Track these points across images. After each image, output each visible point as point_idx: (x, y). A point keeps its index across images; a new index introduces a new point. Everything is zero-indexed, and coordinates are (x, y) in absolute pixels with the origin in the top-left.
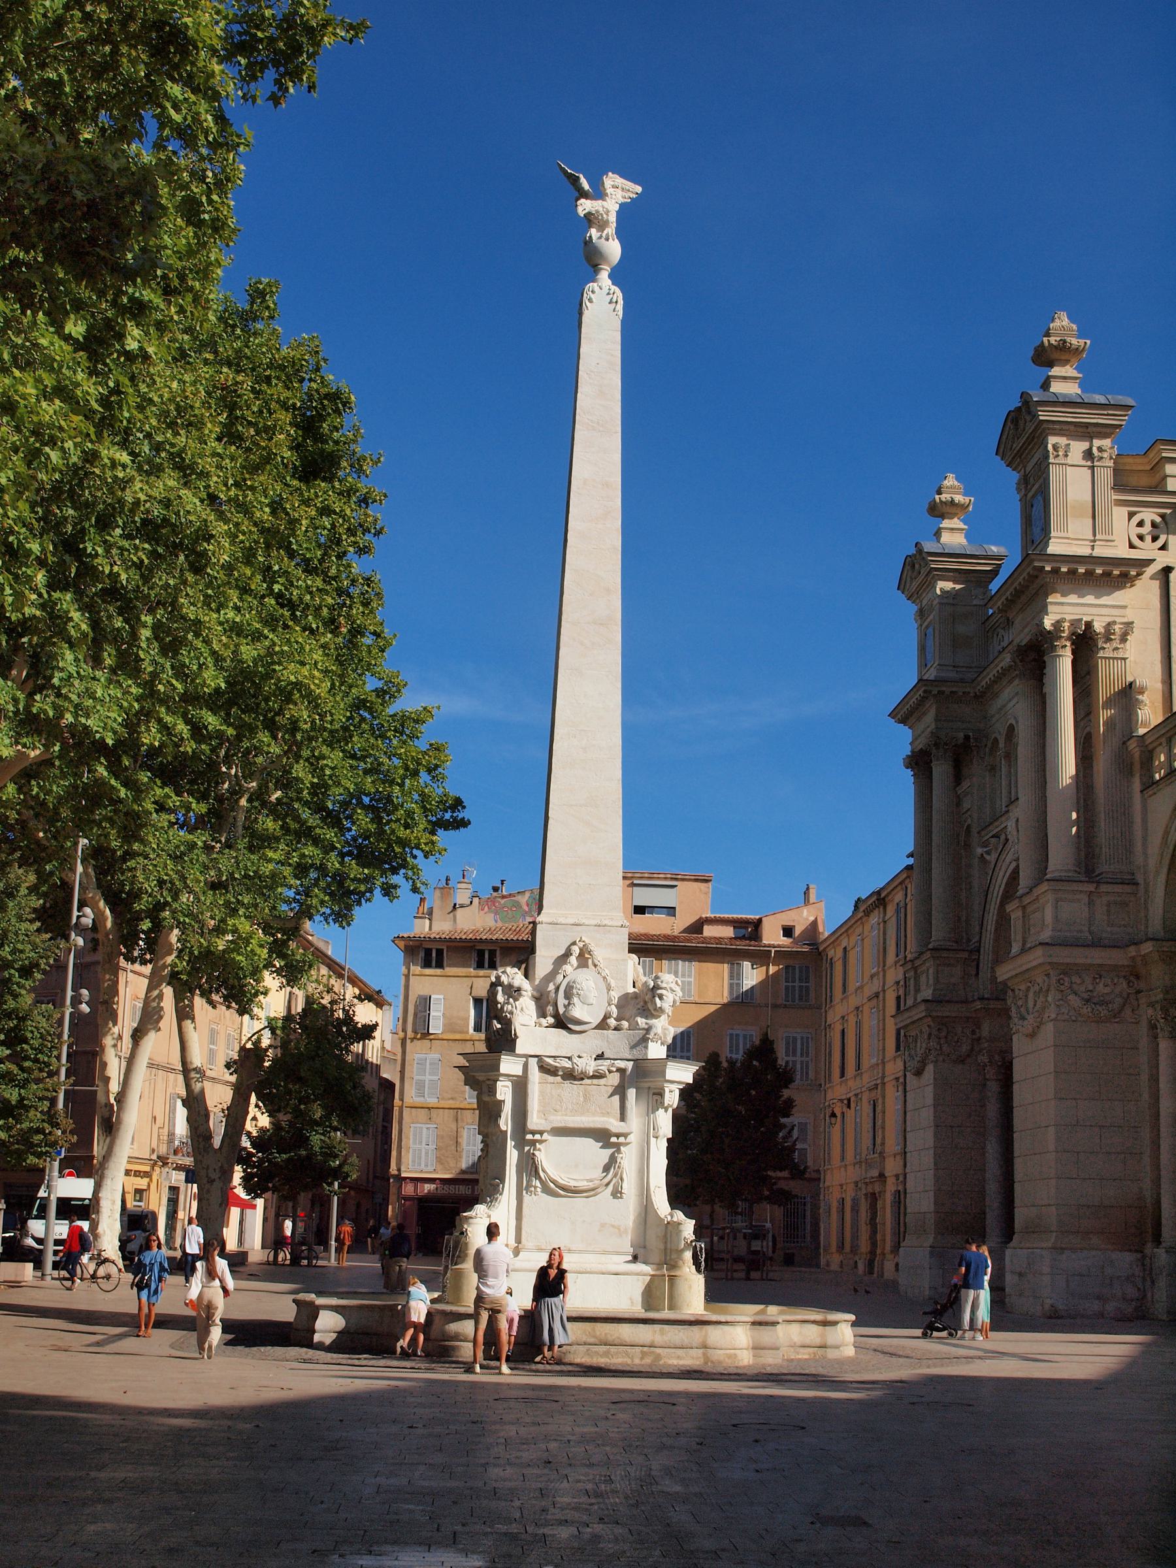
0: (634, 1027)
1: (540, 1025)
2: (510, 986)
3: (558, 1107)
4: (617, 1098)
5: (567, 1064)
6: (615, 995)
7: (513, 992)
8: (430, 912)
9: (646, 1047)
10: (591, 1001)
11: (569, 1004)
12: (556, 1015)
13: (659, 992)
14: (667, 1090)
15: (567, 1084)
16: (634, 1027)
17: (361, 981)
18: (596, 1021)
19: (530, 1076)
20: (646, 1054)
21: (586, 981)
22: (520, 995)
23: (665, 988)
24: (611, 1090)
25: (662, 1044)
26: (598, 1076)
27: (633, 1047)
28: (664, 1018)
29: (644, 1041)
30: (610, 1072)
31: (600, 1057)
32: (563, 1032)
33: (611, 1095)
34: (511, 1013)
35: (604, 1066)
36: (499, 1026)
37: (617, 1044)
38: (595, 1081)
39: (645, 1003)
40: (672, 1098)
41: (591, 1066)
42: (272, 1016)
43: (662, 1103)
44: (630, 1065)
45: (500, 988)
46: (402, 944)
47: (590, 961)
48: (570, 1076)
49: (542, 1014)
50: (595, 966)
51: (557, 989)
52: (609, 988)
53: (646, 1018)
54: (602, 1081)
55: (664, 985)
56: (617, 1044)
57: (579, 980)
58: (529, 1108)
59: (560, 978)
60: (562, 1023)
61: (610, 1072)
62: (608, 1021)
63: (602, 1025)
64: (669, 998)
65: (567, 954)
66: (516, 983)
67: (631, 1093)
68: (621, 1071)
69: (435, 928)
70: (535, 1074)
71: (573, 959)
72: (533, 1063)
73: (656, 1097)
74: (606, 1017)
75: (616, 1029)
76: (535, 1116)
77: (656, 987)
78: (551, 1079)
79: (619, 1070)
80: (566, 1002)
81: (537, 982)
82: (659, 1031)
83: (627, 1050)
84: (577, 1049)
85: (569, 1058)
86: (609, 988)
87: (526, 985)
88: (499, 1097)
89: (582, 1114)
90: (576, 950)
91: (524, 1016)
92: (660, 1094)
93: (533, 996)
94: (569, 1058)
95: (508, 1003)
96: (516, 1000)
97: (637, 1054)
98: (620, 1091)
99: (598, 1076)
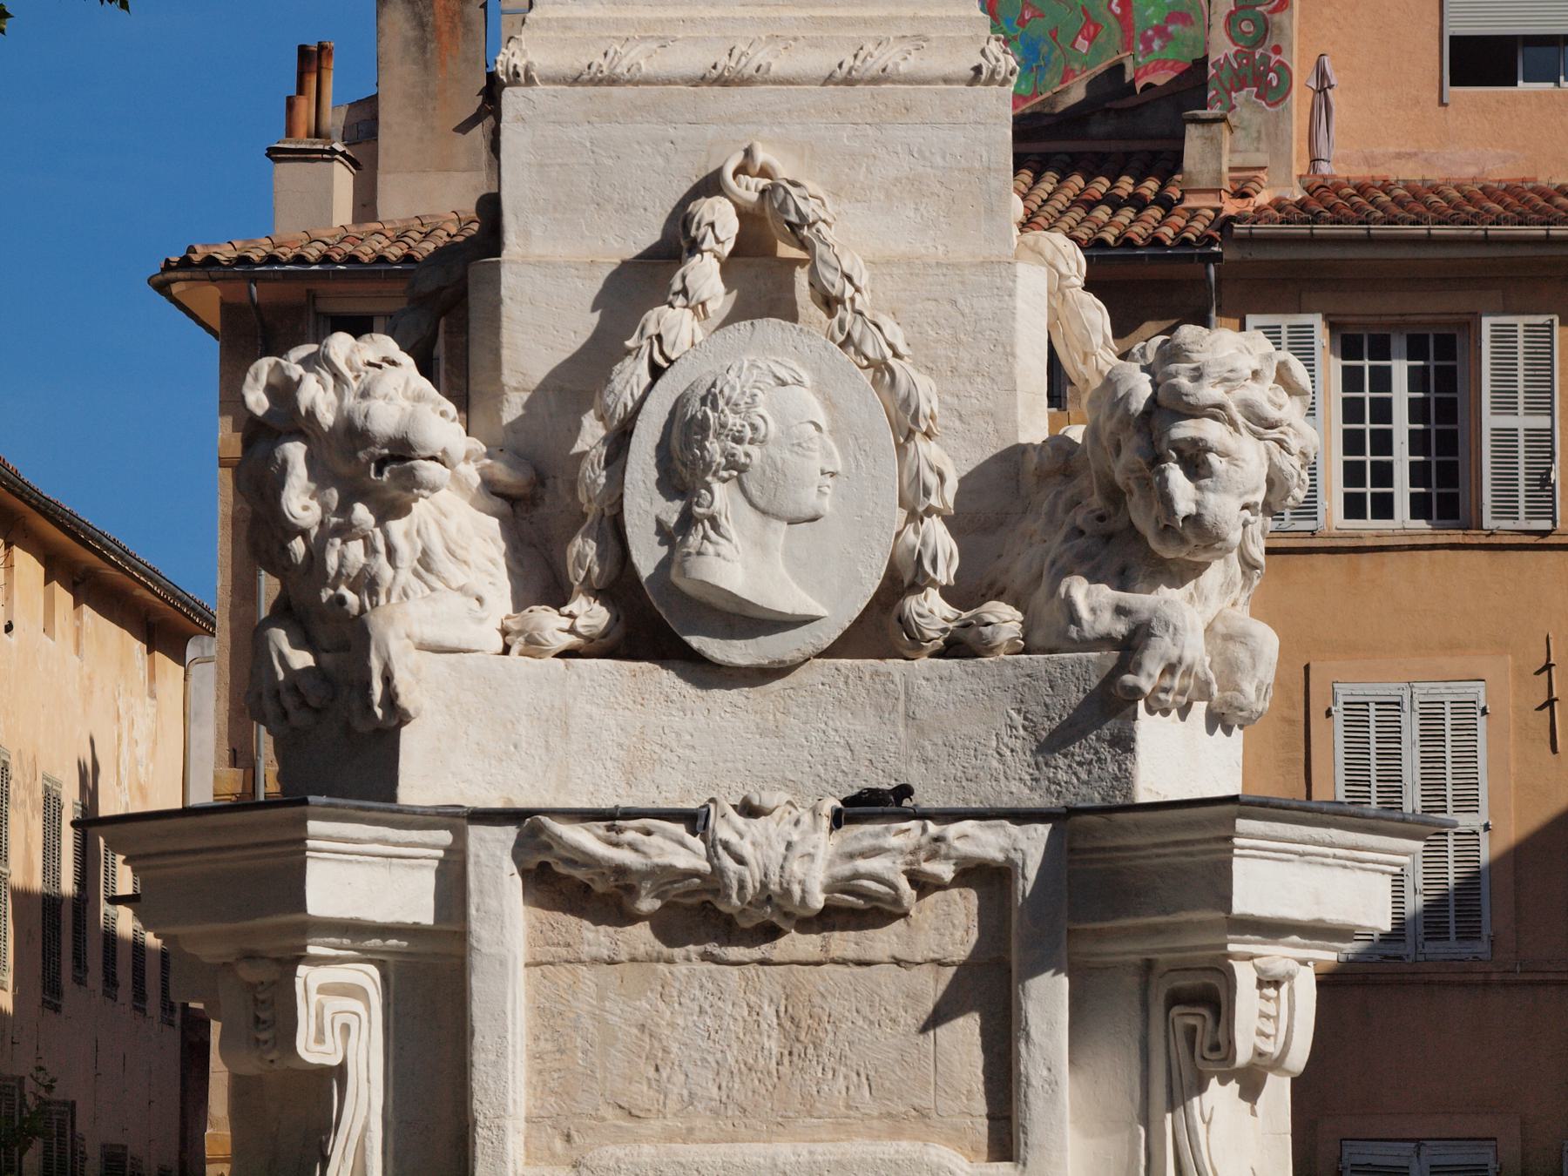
0: (1051, 632)
1: (534, 647)
2: (352, 434)
3: (642, 1094)
4: (966, 1030)
5: (679, 852)
6: (947, 462)
7: (375, 471)
8: (364, 126)
9: (1125, 743)
10: (809, 500)
11: (688, 521)
12: (619, 586)
13: (1185, 430)
14: (1245, 975)
15: (687, 964)
16: (1051, 632)
17: (49, 511)
18: (837, 604)
19: (479, 928)
20: (1125, 779)
21: (780, 389)
22: (411, 482)
23: (1216, 412)
24: (932, 986)
25: (1218, 720)
26: (857, 909)
27: (1054, 743)
28: (1218, 574)
29: (1108, 710)
30: (924, 885)
31: (863, 806)
32: (661, 679)
33: (938, 1017)
34: (367, 583)
35: (888, 851)
36: (302, 659)
37: (961, 730)
38: (843, 942)
39: (1115, 496)
40: (1276, 1013)
41: (814, 861)
42: (756, 802)
43: (1223, 1048)
44: (1032, 843)
45: (295, 452)
46: (208, 298)
47: (801, 277)
48: (706, 915)
49: (541, 581)
50: (829, 303)
51: (620, 440)
52: (907, 425)
53: (1122, 582)
54: (883, 941)
55: (1210, 393)
56: (961, 730)
57: (734, 385)
58: (482, 1107)
59: (631, 376)
60: (657, 626)
61: (924, 885)
62: (912, 604)
63: (879, 630)
64: (1244, 463)
65: (678, 242)
66: (385, 418)
67: (1047, 1000)
68: (986, 878)
69: (395, 205)
70: (506, 919)
71: (704, 274)
72: (492, 852)
73: (1183, 1018)
74: (902, 580)
75: (959, 646)
76: (515, 1146)
77: (1168, 406)
78: (595, 937)
79: (975, 873)
80: (672, 512)
81: (512, 409)
82: (1195, 649)
83: (1020, 763)
84: (741, 766)
85: (695, 820)
86: (907, 425)
87: (438, 424)
88: (311, 1049)
89: (781, 1125)
90: (721, 220)
91: (443, 595)
92: (1212, 998)
93: (490, 487)
94: (695, 820)
95: (346, 531)
96: (389, 510)
97: (1074, 780)
98: (984, 992)
99: (857, 909)
